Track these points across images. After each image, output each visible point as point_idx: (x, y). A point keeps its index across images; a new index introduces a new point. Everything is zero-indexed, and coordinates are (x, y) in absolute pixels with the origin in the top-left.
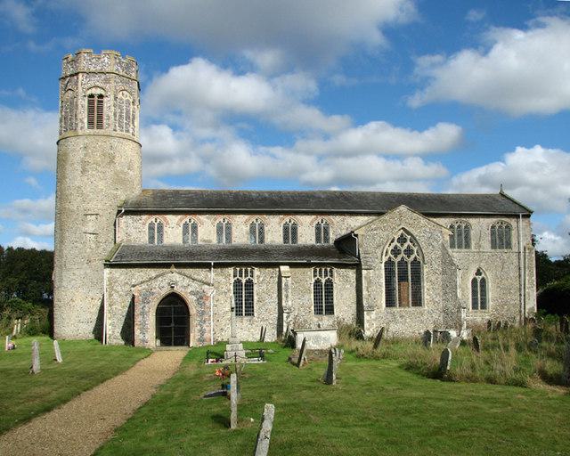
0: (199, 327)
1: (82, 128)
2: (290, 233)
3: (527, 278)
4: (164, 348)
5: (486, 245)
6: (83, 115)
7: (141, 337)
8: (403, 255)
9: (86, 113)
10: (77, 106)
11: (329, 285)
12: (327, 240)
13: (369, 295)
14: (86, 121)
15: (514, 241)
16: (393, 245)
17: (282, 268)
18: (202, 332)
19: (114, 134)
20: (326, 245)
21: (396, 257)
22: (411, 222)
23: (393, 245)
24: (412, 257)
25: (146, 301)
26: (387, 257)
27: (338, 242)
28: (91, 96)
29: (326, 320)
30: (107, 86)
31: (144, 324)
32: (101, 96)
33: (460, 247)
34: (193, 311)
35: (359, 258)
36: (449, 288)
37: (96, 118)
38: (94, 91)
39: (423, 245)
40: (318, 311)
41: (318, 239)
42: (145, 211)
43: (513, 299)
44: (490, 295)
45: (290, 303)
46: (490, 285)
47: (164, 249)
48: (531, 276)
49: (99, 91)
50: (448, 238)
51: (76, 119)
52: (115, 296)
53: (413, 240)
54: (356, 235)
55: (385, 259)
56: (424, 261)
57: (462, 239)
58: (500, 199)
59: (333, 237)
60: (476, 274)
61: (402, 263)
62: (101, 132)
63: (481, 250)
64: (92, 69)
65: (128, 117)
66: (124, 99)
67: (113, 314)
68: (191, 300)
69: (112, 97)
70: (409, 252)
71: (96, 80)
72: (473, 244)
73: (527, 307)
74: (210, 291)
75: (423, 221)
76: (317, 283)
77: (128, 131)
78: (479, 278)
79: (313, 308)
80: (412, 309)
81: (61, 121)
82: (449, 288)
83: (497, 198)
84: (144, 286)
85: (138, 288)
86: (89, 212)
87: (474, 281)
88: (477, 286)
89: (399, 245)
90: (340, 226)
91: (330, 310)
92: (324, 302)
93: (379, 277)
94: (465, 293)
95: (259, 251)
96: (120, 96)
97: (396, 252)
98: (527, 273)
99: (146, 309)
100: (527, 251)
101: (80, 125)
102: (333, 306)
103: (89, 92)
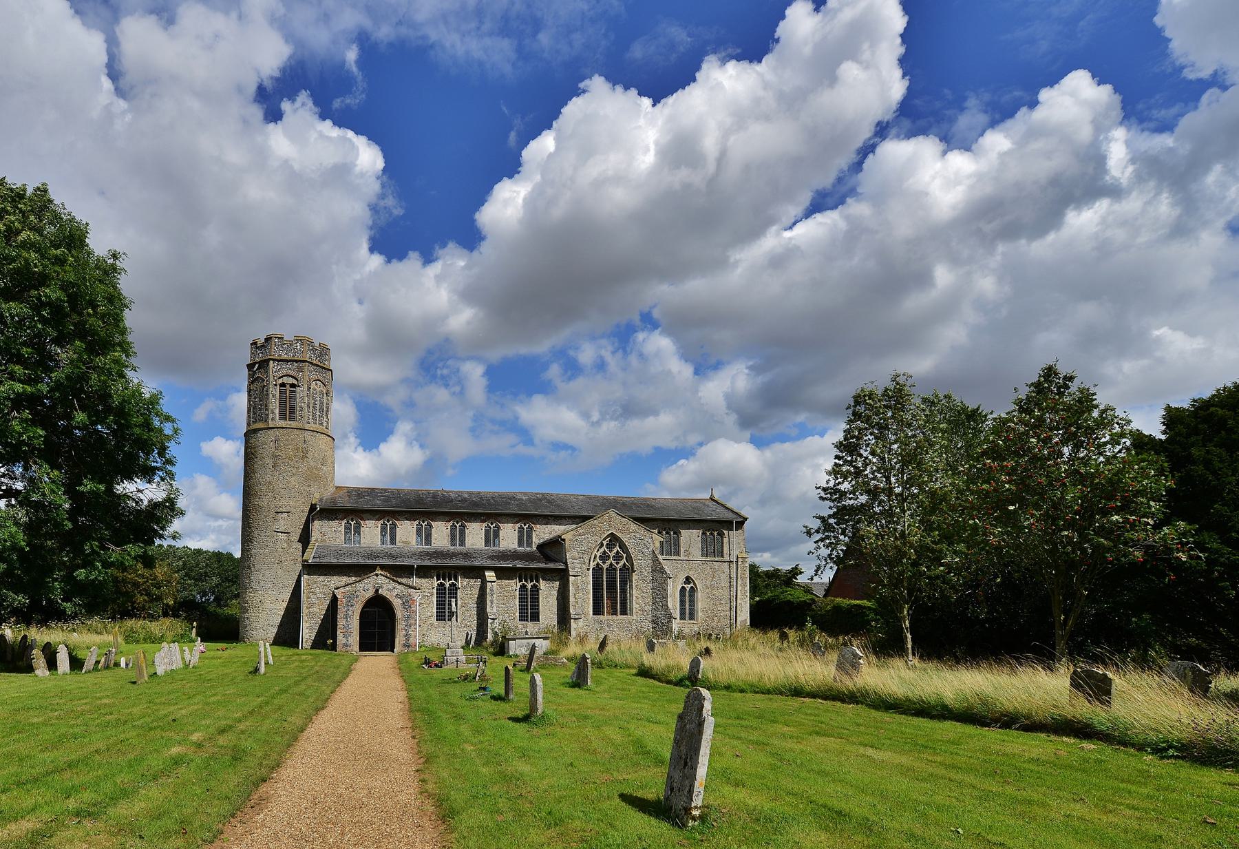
0: (404, 632)
1: (273, 419)
2: (458, 536)
3: (739, 588)
4: (399, 640)
5: (696, 553)
6: (274, 405)
7: (344, 641)
8: (611, 555)
9: (278, 403)
10: (268, 395)
11: (536, 590)
12: (529, 544)
13: (577, 602)
14: (277, 411)
15: (726, 550)
16: (602, 550)
17: (487, 573)
18: (407, 637)
19: (307, 426)
20: (528, 549)
21: (604, 563)
22: (621, 526)
23: (602, 550)
24: (621, 563)
25: (349, 603)
26: (596, 563)
27: (540, 547)
28: (283, 385)
29: (532, 627)
30: (300, 376)
31: (347, 628)
32: (293, 385)
33: (615, 613)
34: (400, 613)
35: (566, 563)
36: (660, 595)
37: (289, 411)
38: (285, 380)
39: (631, 551)
40: (523, 617)
41: (520, 543)
42: (504, 514)
43: (723, 610)
44: (700, 605)
45: (495, 609)
46: (700, 595)
47: (362, 550)
48: (744, 586)
49: (291, 380)
50: (658, 545)
51: (267, 409)
52: (313, 598)
53: (623, 546)
54: (564, 540)
55: (593, 565)
56: (633, 568)
57: (672, 548)
58: (711, 504)
59: (536, 541)
60: (685, 583)
61: (611, 568)
62: (293, 424)
63: (691, 558)
64: (284, 357)
65: (321, 409)
66: (318, 389)
67: (309, 615)
68: (397, 603)
69: (306, 386)
70: (618, 558)
71: (288, 368)
72: (682, 550)
73: (739, 619)
74: (417, 596)
75: (633, 526)
76: (523, 587)
77: (321, 424)
78: (688, 587)
79: (518, 614)
80: (620, 617)
81: (249, 411)
82: (660, 595)
83: (707, 503)
84: (347, 588)
85: (342, 590)
86: (281, 510)
87: (683, 589)
88: (685, 595)
89: (607, 550)
90: (543, 533)
91: (535, 617)
92: (530, 611)
93: (586, 583)
94: (674, 603)
95: (461, 554)
96: (313, 385)
97: (604, 557)
98: (739, 583)
99: (350, 613)
100: (740, 560)
101: (271, 416)
102: (538, 613)
103: (280, 381)
